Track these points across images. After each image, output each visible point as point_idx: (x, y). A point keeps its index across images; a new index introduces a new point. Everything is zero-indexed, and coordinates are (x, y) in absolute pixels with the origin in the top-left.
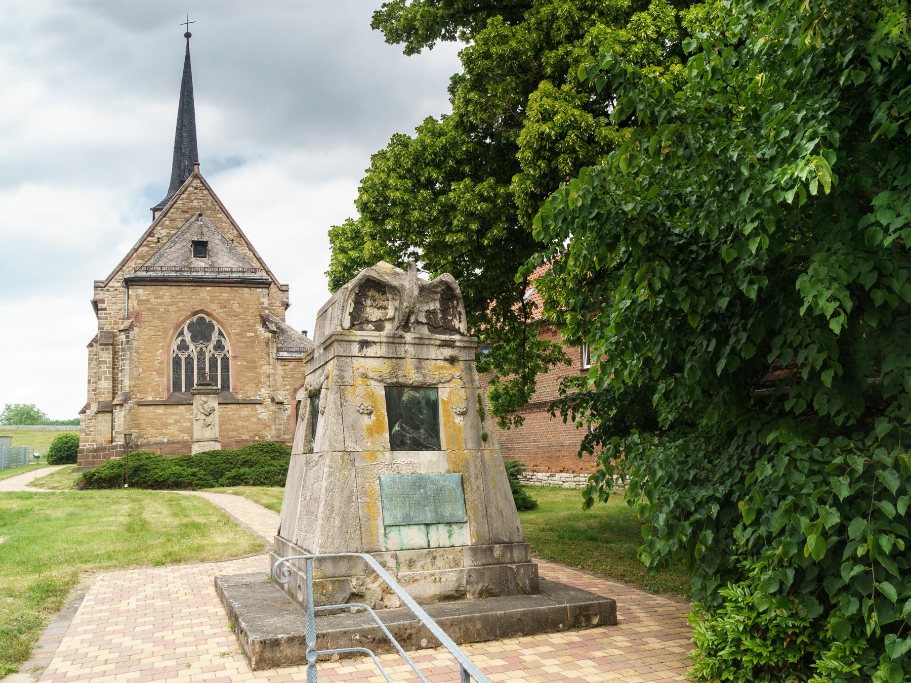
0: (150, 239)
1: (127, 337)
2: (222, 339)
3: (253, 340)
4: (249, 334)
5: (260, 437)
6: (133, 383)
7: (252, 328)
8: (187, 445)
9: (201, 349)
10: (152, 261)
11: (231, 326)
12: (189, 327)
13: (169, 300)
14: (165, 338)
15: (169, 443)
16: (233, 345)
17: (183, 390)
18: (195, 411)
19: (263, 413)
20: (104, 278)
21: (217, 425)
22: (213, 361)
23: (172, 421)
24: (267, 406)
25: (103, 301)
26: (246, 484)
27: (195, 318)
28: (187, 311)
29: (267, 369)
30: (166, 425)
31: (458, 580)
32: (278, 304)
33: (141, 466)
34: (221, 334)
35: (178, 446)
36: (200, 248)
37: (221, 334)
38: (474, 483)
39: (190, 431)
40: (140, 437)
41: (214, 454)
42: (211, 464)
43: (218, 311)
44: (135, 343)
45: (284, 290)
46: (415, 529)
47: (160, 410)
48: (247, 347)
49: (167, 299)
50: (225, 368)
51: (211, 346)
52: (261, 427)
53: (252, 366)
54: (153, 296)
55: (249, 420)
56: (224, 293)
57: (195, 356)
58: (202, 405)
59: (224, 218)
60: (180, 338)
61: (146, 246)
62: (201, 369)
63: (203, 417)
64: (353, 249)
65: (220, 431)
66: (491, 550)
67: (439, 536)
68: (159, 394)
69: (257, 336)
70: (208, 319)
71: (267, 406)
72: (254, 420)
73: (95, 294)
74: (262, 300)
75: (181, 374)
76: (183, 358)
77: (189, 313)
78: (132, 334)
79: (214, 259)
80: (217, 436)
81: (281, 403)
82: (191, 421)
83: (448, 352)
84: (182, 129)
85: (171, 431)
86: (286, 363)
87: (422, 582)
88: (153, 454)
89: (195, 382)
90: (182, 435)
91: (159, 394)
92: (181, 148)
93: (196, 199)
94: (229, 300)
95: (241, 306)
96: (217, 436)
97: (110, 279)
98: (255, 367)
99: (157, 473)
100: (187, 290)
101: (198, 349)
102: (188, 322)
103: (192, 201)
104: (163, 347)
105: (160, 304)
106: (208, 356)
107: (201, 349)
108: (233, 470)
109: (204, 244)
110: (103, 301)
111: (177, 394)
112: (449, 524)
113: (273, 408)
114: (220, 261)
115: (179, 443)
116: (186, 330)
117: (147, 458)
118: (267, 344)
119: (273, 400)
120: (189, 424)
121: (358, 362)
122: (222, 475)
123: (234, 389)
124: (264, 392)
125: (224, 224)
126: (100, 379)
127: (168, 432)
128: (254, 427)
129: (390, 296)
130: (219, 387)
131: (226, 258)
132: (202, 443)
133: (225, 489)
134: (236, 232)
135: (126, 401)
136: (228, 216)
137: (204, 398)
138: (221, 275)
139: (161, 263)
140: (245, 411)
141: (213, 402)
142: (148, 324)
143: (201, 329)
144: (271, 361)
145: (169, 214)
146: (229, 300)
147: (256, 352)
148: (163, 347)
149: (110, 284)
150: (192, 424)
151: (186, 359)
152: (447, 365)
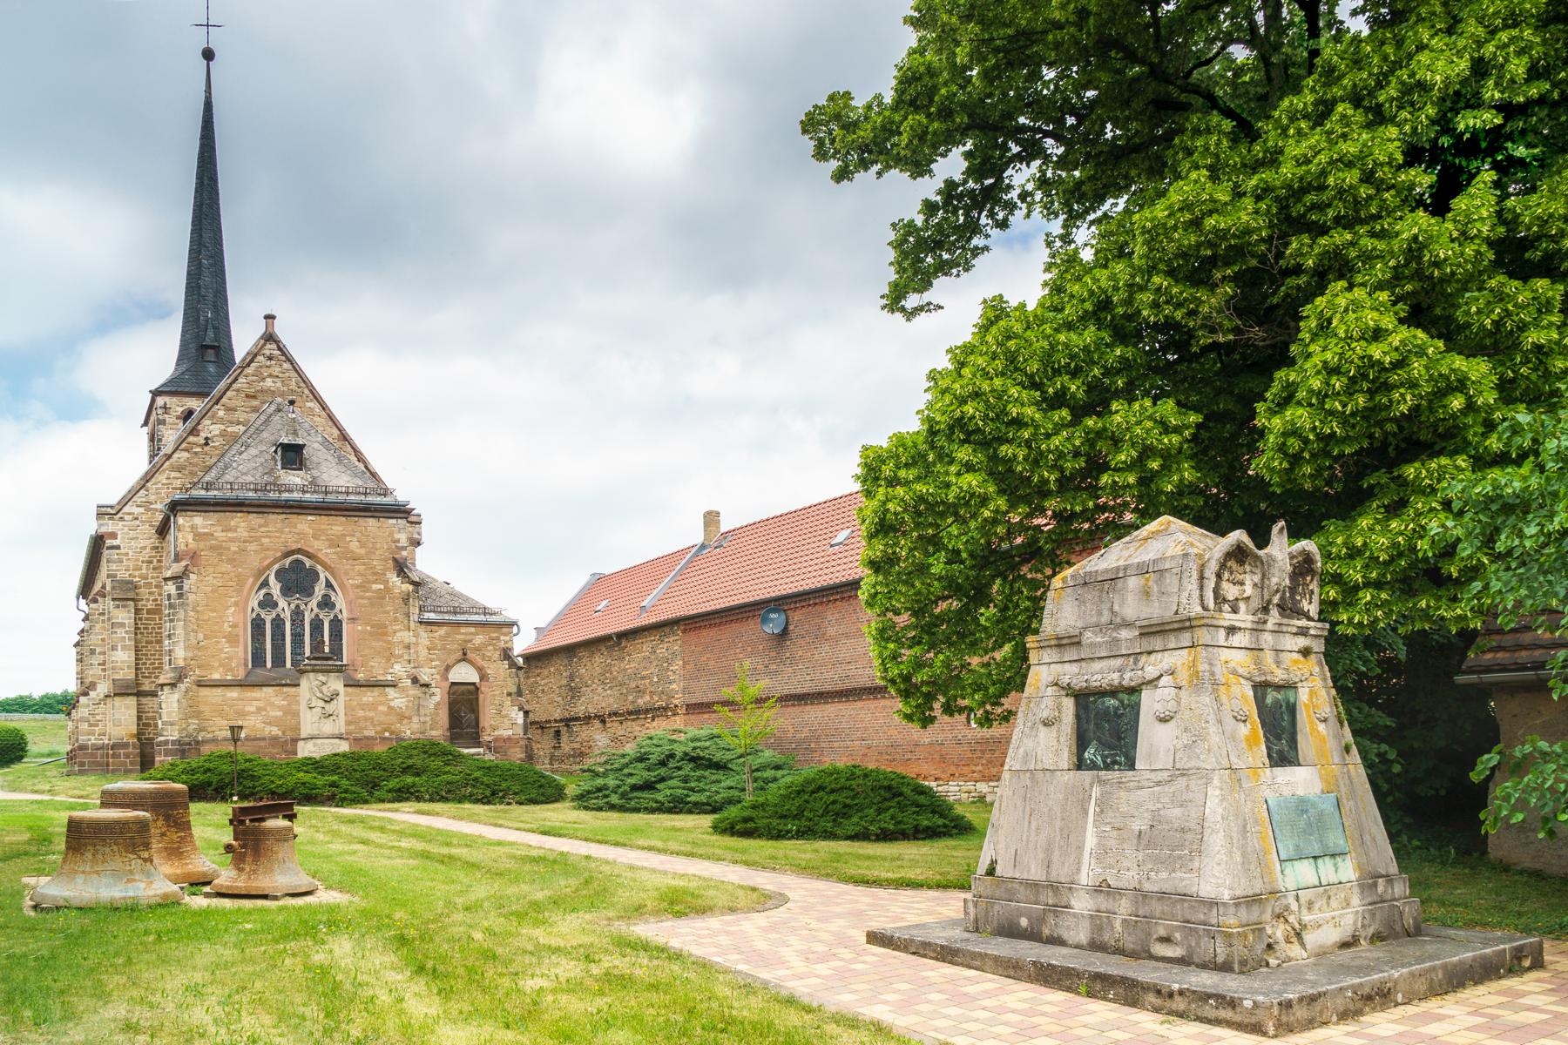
0: (191, 439)
1: (180, 588)
3: (380, 595)
4: (375, 587)
5: (392, 733)
6: (190, 654)
7: (380, 577)
10: (213, 473)
11: (347, 573)
12: (278, 574)
14: (239, 592)
16: (349, 603)
17: (269, 665)
19: (397, 700)
20: (113, 502)
21: (342, 715)
22: (317, 625)
23: (253, 709)
24: (404, 689)
27: (288, 561)
29: (407, 636)
31: (1355, 923)
34: (329, 585)
35: (262, 743)
36: (292, 455)
37: (329, 585)
38: (1348, 805)
40: (201, 730)
44: (191, 597)
46: (1305, 862)
47: (233, 694)
48: (372, 605)
49: (242, 533)
50: (337, 634)
51: (314, 603)
52: (393, 718)
53: (380, 631)
55: (375, 709)
56: (337, 526)
57: (287, 616)
59: (317, 409)
60: (263, 592)
61: (186, 450)
63: (322, 704)
64: (918, 479)
66: (1375, 885)
67: (1327, 870)
68: (231, 670)
69: (388, 589)
70: (308, 563)
71: (404, 689)
73: (100, 526)
74: (396, 536)
78: (191, 582)
79: (315, 473)
81: (427, 686)
83: (1302, 642)
87: (1325, 927)
90: (268, 729)
91: (231, 670)
92: (199, 287)
93: (270, 376)
97: (125, 501)
98: (386, 634)
100: (276, 520)
102: (276, 567)
103: (263, 379)
104: (236, 604)
105: (231, 540)
106: (308, 618)
107: (298, 607)
109: (298, 449)
110: (113, 535)
111: (259, 671)
112: (1333, 856)
113: (415, 691)
114: (325, 476)
116: (272, 579)
118: (406, 600)
119: (415, 680)
121: (1225, 654)
124: (399, 669)
126: (114, 648)
128: (383, 718)
129: (1248, 568)
131: (334, 472)
134: (336, 432)
135: (180, 679)
136: (324, 407)
137: (321, 677)
138: (331, 498)
139: (228, 478)
141: (335, 684)
143: (298, 578)
145: (224, 400)
148: (236, 604)
149: (126, 509)
152: (1298, 657)
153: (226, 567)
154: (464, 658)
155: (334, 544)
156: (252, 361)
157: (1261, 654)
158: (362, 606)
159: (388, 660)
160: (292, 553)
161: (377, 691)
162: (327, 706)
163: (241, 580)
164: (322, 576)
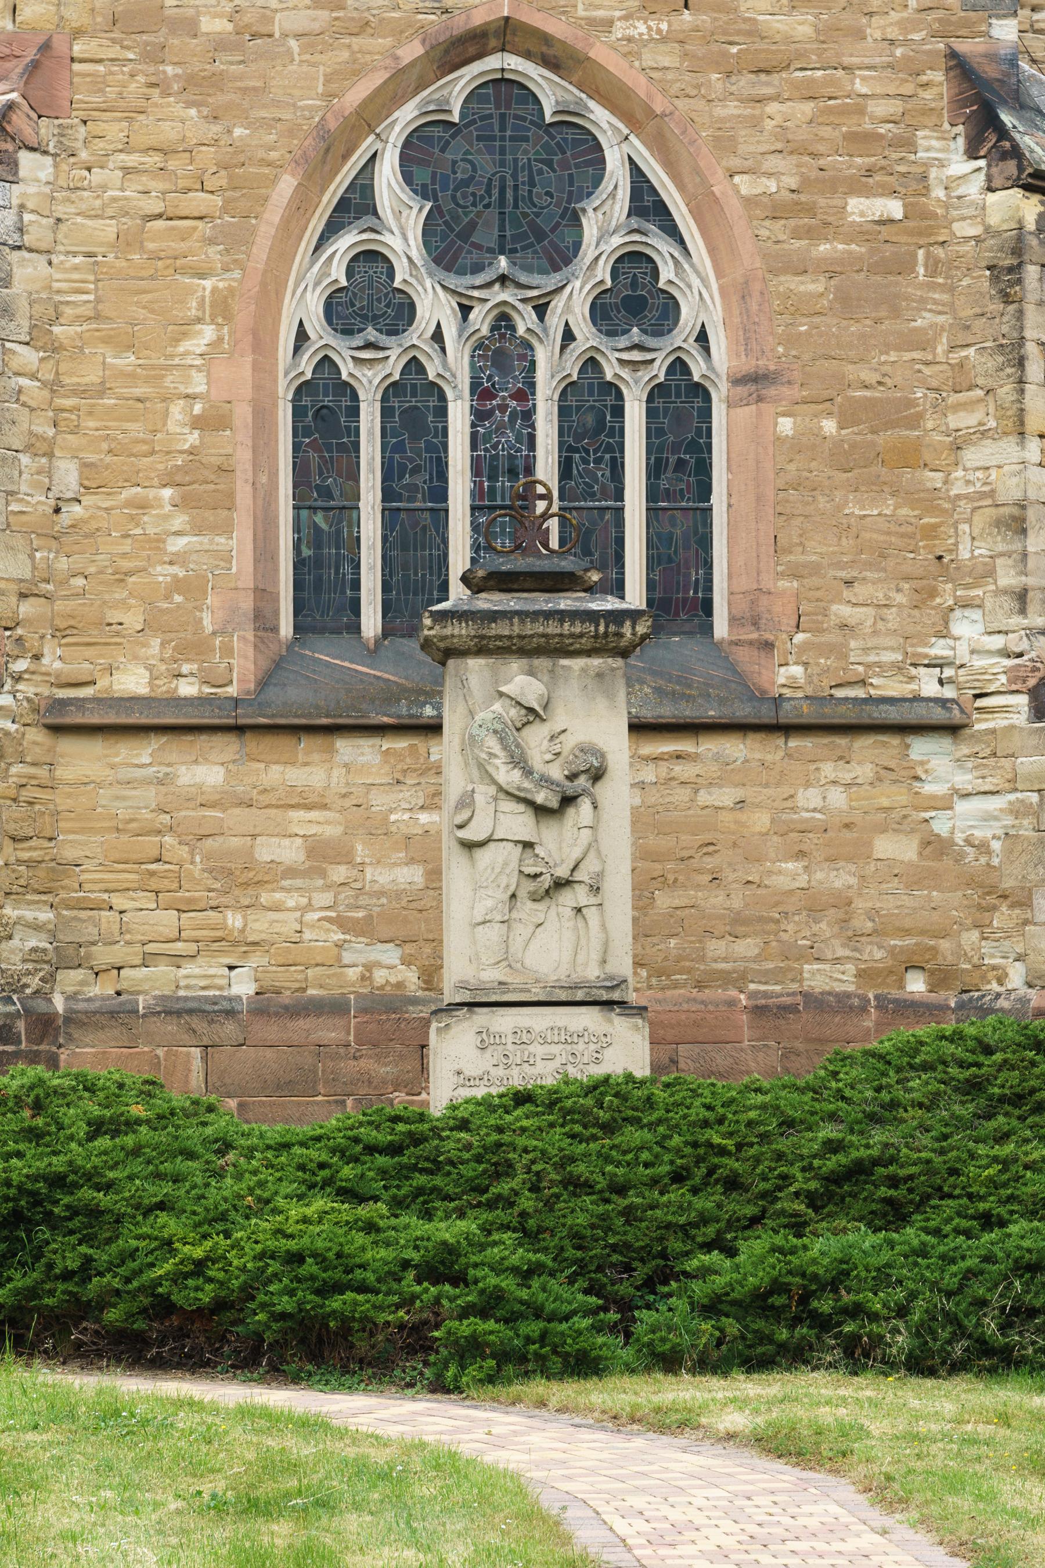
2: (661, 247)
3: (889, 254)
4: (862, 209)
5: (940, 978)
8: (400, 1026)
9: (503, 321)
11: (724, 143)
12: (415, 153)
14: (235, 241)
15: (266, 1005)
16: (739, 294)
17: (371, 622)
18: (456, 780)
22: (590, 410)
23: (289, 852)
24: (997, 749)
26: (859, 1356)
27: (457, 89)
28: (400, 32)
30: (242, 879)
33: (57, 1181)
34: (647, 205)
35: (329, 1032)
37: (647, 205)
39: (415, 922)
41: (598, 1108)
42: (577, 1186)
47: (205, 770)
48: (846, 303)
51: (573, 305)
52: (951, 901)
53: (887, 443)
55: (860, 853)
57: (455, 369)
58: (511, 737)
60: (346, 242)
62: (502, 469)
63: (518, 823)
65: (641, 932)
68: (194, 647)
69: (923, 222)
70: (550, 93)
72: (897, 848)
75: (351, 508)
76: (369, 383)
77: (412, 51)
80: (622, 965)
82: (423, 851)
85: (287, 924)
88: (150, 1089)
89: (459, 557)
90: (359, 953)
91: (194, 647)
96: (622, 965)
98: (910, 457)
99: (787, 714)
101: (480, 319)
102: (406, 116)
104: (221, 308)
107: (503, 321)
108: (754, 1247)
111: (327, 655)
115: (334, 1008)
116: (388, 176)
117: (97, 1128)
118: (1006, 277)
120: (412, 876)
122: (662, 1276)
123: (747, 618)
127: (260, 926)
128: (896, 901)
130: (635, 596)
132: (505, 1021)
133: (682, 1391)
137: (522, 682)
140: (831, 783)
141: (590, 714)
142: (114, 130)
147: (922, 342)
148: (221, 308)
150: (435, 875)
151: (392, 391)
153: (180, 120)
157: (747, 365)
158: (799, 307)
159: (925, 595)
160: (470, 45)
163: (244, 190)
164: (614, 160)
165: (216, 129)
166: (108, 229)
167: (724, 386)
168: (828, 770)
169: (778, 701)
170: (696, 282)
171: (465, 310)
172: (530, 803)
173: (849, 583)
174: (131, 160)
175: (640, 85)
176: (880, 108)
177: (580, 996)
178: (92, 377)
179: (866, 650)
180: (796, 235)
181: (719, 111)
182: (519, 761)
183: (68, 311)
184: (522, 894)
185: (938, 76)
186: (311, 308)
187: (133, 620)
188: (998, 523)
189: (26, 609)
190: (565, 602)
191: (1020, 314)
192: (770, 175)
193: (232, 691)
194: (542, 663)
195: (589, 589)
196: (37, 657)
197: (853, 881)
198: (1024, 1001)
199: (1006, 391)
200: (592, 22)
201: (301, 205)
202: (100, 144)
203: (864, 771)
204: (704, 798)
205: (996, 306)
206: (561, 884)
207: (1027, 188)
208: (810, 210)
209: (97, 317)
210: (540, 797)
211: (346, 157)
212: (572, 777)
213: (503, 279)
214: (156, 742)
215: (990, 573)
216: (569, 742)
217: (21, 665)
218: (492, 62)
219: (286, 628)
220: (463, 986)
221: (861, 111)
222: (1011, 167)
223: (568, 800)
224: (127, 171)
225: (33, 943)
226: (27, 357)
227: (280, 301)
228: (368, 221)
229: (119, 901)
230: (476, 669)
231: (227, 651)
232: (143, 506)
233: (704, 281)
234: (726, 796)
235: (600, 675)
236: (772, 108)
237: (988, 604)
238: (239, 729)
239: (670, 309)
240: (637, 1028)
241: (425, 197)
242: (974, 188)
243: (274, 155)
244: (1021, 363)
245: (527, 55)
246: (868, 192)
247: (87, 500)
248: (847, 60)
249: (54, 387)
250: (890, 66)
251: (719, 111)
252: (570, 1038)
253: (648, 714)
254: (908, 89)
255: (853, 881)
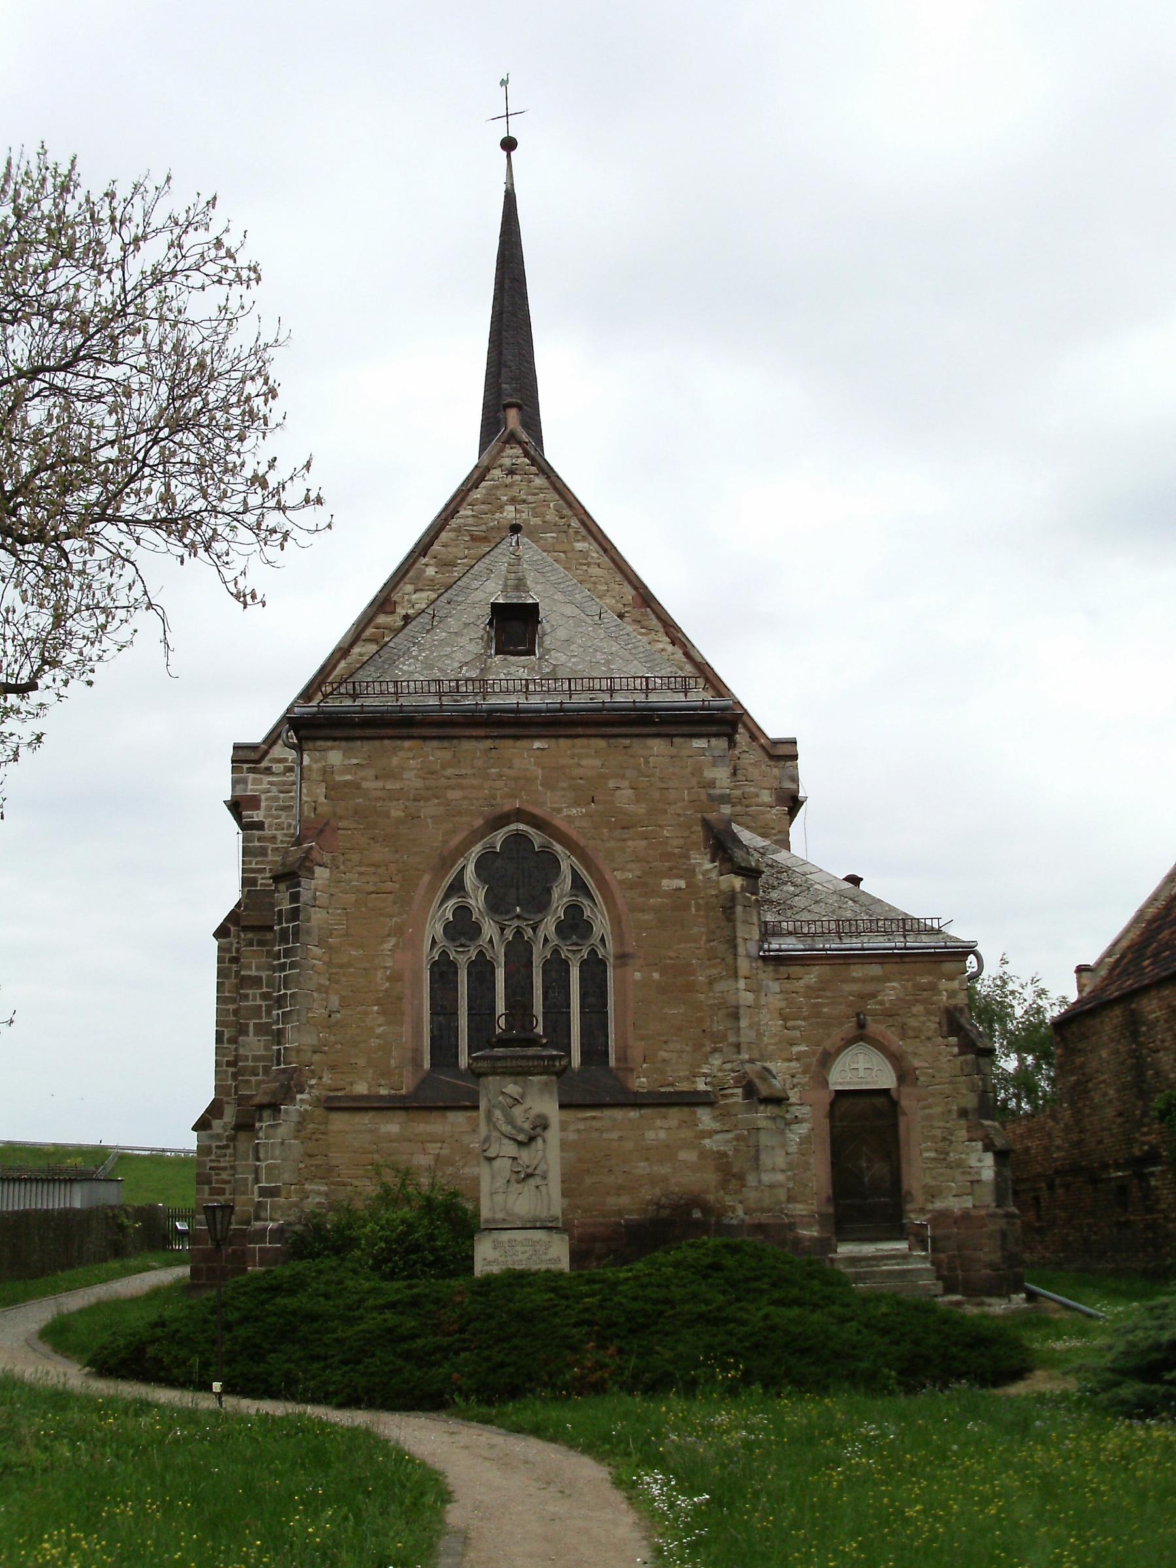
0: (382, 619)
4: (668, 884)
13: (419, 783)
25: (254, 802)
27: (498, 838)
32: (766, 797)
36: (515, 625)
37: (579, 885)
43: (568, 814)
45: (783, 753)
47: (392, 1126)
49: (412, 780)
51: (549, 926)
54: (371, 773)
56: (587, 756)
59: (595, 553)
60: (451, 903)
63: (510, 1149)
70: (538, 838)
72: (688, 1156)
73: (235, 783)
74: (709, 774)
76: (463, 960)
77: (479, 822)
81: (778, 1101)
84: (499, 374)
86: (795, 970)
93: (513, 501)
94: (605, 777)
95: (640, 795)
98: (691, 988)
100: (474, 749)
102: (477, 850)
103: (501, 508)
105: (393, 796)
107: (519, 932)
119: (750, 1091)
123: (622, 1058)
125: (595, 571)
132: (505, 1236)
134: (629, 593)
140: (660, 1128)
142: (356, 857)
143: (520, 870)
144: (743, 965)
145: (436, 547)
146: (605, 777)
151: (472, 964)
153: (380, 853)
154: (861, 1035)
155: (586, 794)
156: (482, 478)
161: (675, 1116)
162: (525, 1156)
164: (564, 866)
165: (397, 856)
166: (352, 898)
167: (612, 960)
168: (658, 1123)
169: (636, 1093)
170: (599, 916)
171: (502, 930)
172: (515, 1140)
173: (666, 1042)
174: (363, 869)
175: (574, 835)
176: (675, 842)
177: (538, 1225)
178: (345, 960)
179: (673, 1071)
180: (640, 896)
181: (608, 845)
182: (510, 1121)
183: (335, 932)
184: (513, 1180)
185: (699, 828)
186: (439, 929)
187: (362, 1062)
188: (728, 1015)
189: (316, 1057)
190: (531, 1051)
191: (734, 927)
192: (629, 871)
193: (403, 1092)
194: (519, 1078)
195: (544, 1046)
196: (320, 1078)
197: (670, 1170)
198: (743, 1221)
199: (730, 959)
200: (554, 809)
201: (432, 888)
202: (349, 863)
203: (674, 1123)
204: (605, 1136)
205: (723, 924)
206: (529, 1175)
207: (736, 873)
208: (645, 885)
209: (347, 935)
210: (520, 1138)
211: (452, 867)
212: (534, 1129)
213: (518, 917)
214: (371, 1114)
215: (725, 1037)
216: (533, 1112)
217: (313, 1082)
218: (513, 827)
219: (427, 1065)
220: (487, 1221)
221: (667, 844)
222: (729, 866)
223: (532, 1139)
224: (361, 874)
225: (317, 1200)
226: (318, 951)
227: (424, 925)
228: (462, 894)
229: (356, 1182)
230: (492, 1081)
231: (401, 1076)
232: (366, 1013)
233: (604, 917)
234: (615, 1135)
235: (546, 1084)
236: (630, 843)
237: (725, 1050)
238: (406, 1109)
239: (589, 927)
240: (563, 1239)
241: (486, 883)
242: (714, 875)
243: (421, 867)
244: (735, 947)
245: (527, 824)
246: (671, 877)
247: (342, 1012)
248: (661, 823)
249: (329, 964)
250: (679, 825)
251: (608, 845)
252: (534, 1243)
253: (566, 1100)
254: (686, 834)
255: (670, 1170)
